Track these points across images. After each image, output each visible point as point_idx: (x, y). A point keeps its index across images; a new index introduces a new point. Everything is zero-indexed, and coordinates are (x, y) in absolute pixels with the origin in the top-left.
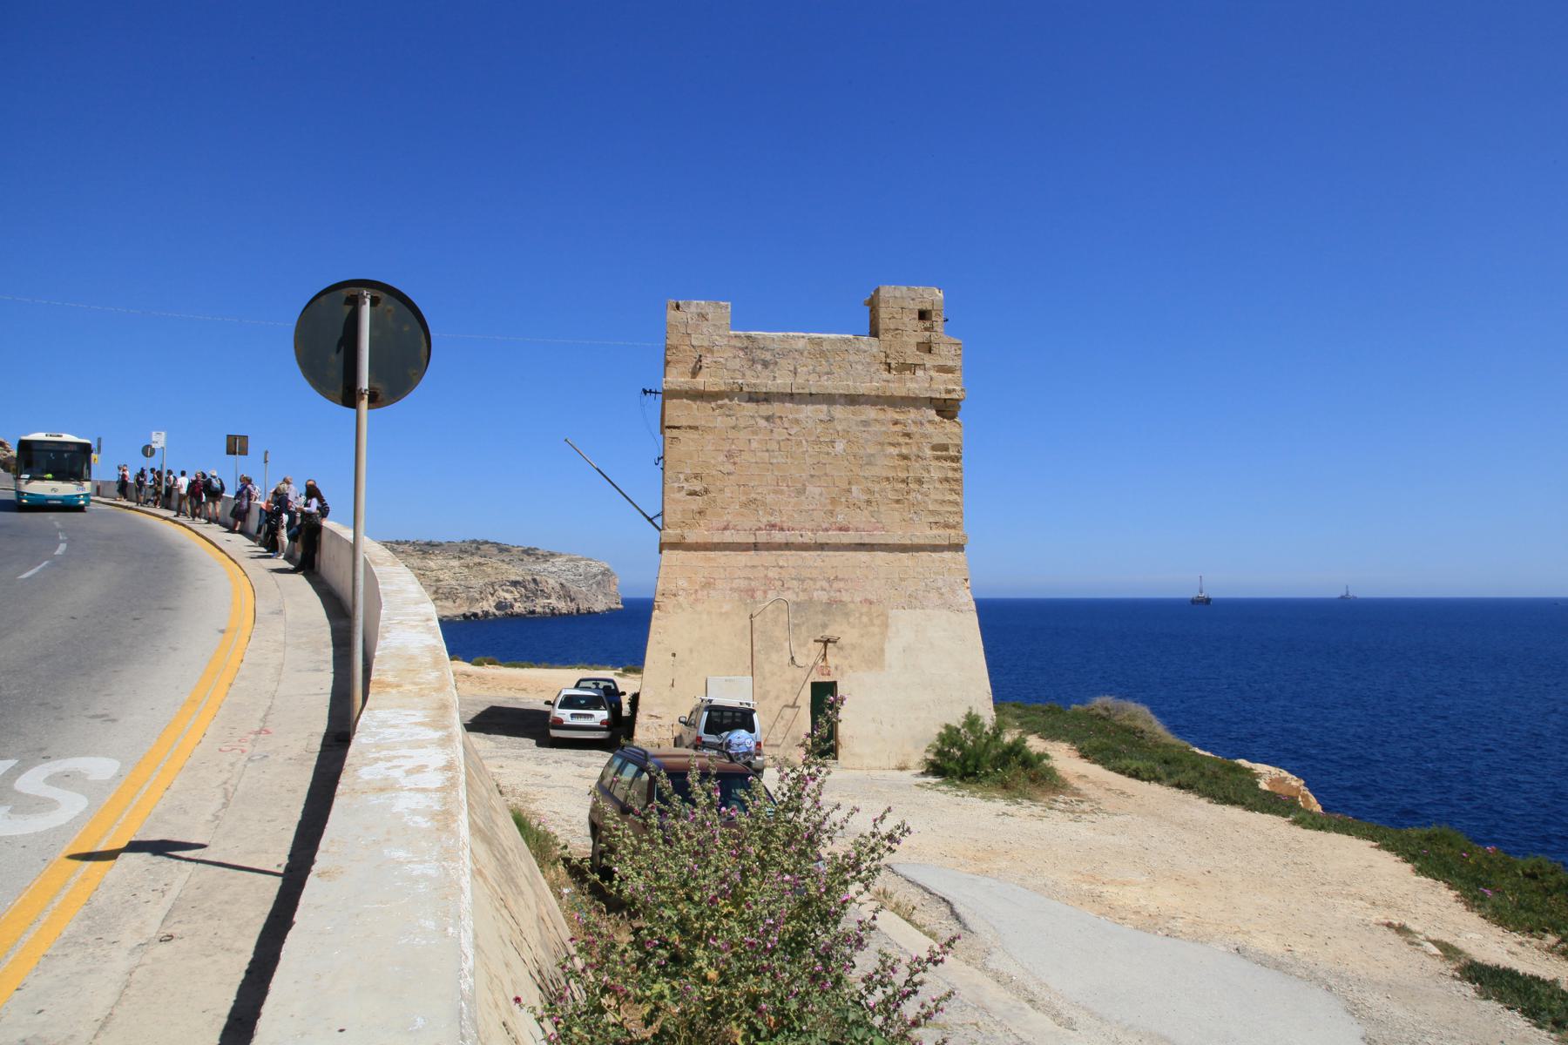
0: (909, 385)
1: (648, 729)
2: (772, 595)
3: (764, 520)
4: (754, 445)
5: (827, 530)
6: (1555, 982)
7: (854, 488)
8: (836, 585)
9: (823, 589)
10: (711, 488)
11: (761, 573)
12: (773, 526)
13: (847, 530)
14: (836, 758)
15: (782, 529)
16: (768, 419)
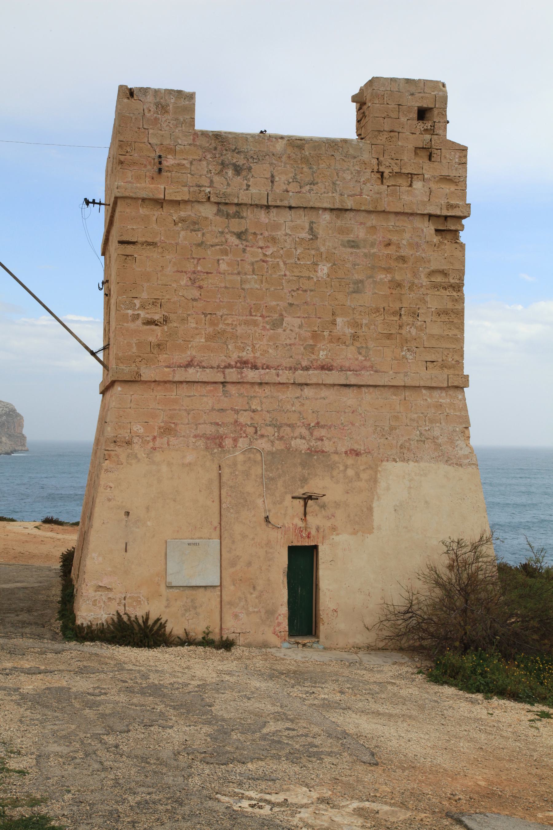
0: (406, 198)
1: (95, 603)
2: (243, 443)
3: (235, 356)
4: (223, 267)
5: (307, 369)
6: (543, 706)
7: (339, 320)
8: (318, 433)
9: (302, 437)
10: (172, 316)
11: (230, 417)
12: (245, 363)
13: (330, 369)
14: (63, 553)
15: (255, 367)
16: (239, 236)
